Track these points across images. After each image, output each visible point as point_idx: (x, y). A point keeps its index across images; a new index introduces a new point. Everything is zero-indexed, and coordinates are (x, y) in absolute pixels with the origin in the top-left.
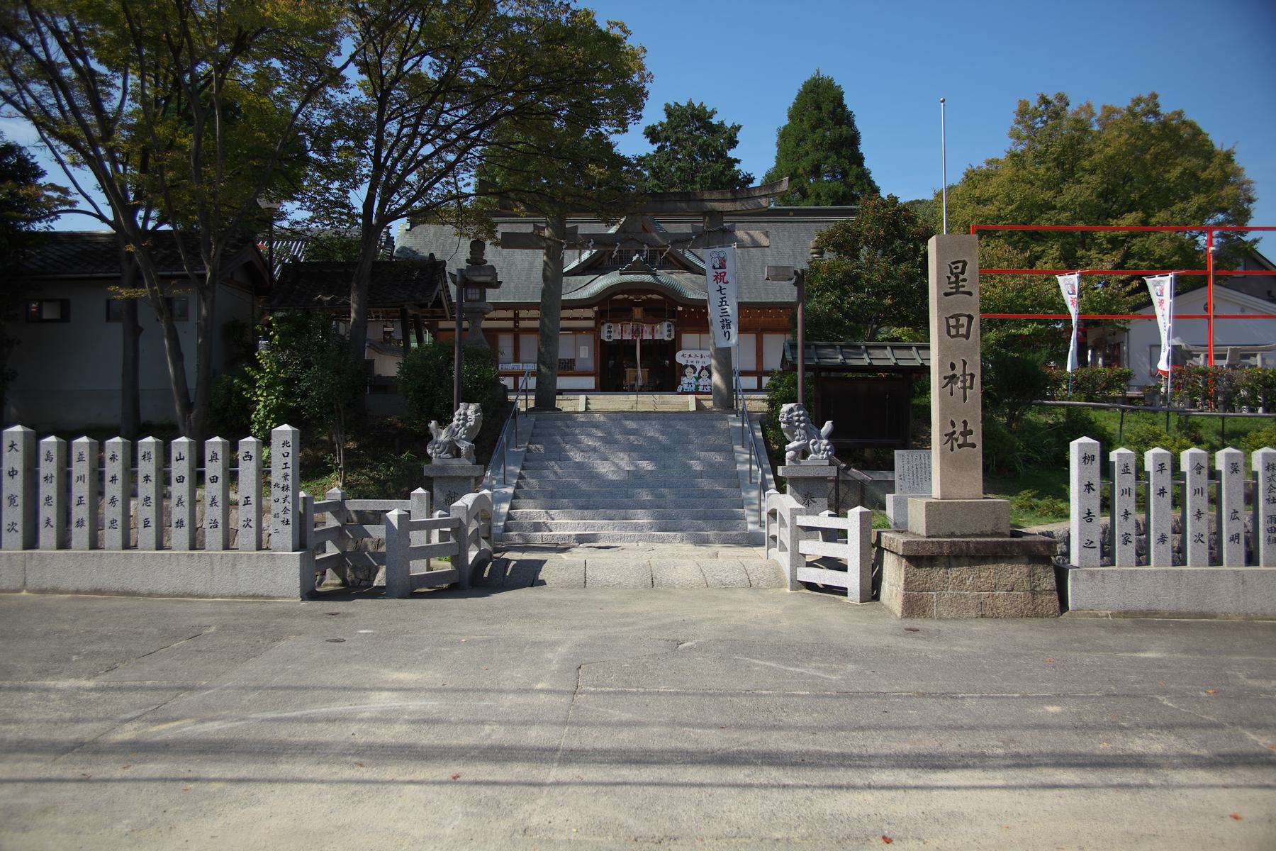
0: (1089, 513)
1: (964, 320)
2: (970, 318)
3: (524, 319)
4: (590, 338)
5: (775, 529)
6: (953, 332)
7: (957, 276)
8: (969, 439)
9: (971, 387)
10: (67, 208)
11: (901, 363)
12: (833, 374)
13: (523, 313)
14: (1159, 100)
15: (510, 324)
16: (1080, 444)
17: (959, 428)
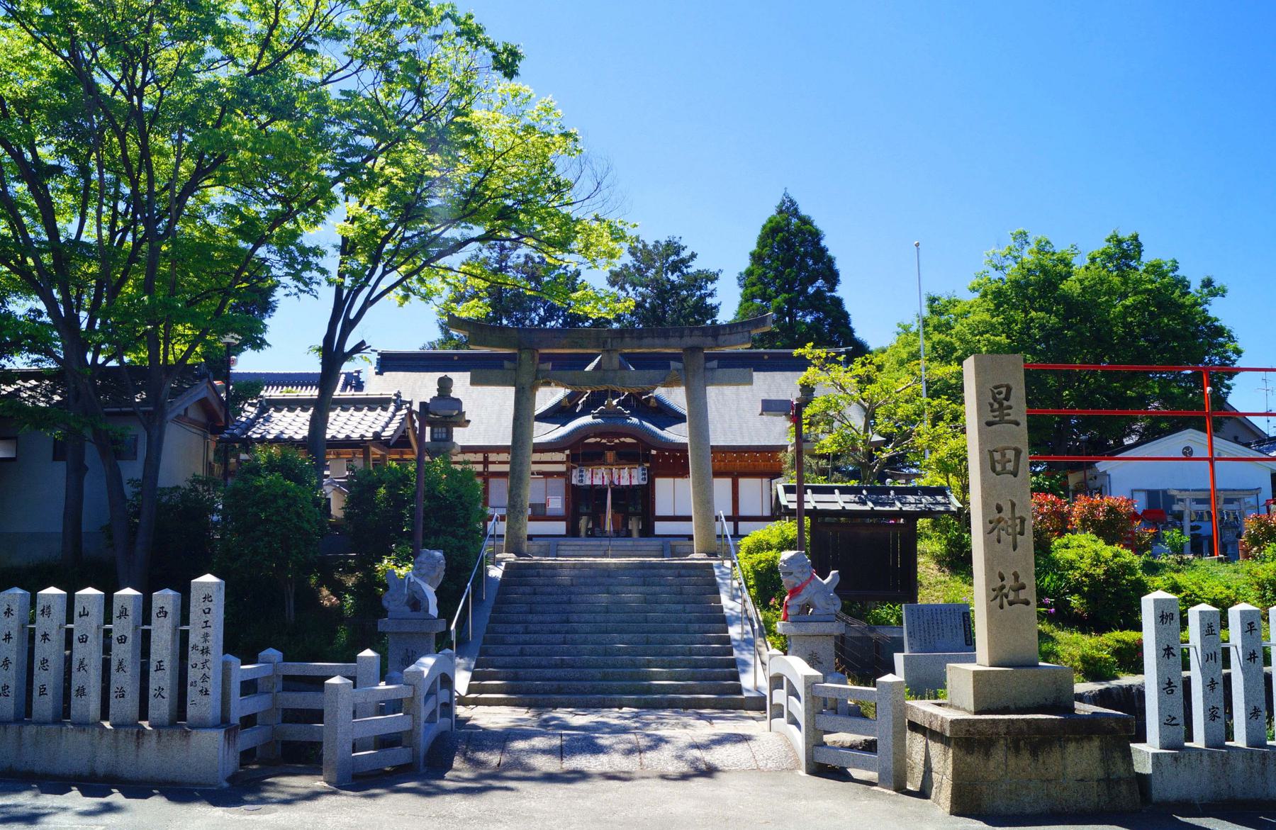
0: (1170, 683)
1: (1010, 454)
2: (1018, 452)
3: (494, 463)
5: (780, 696)
6: (999, 468)
8: (1023, 595)
9: (1022, 533)
10: (522, 774)
12: (827, 519)
15: (480, 468)
16: (1156, 601)
17: (1009, 582)
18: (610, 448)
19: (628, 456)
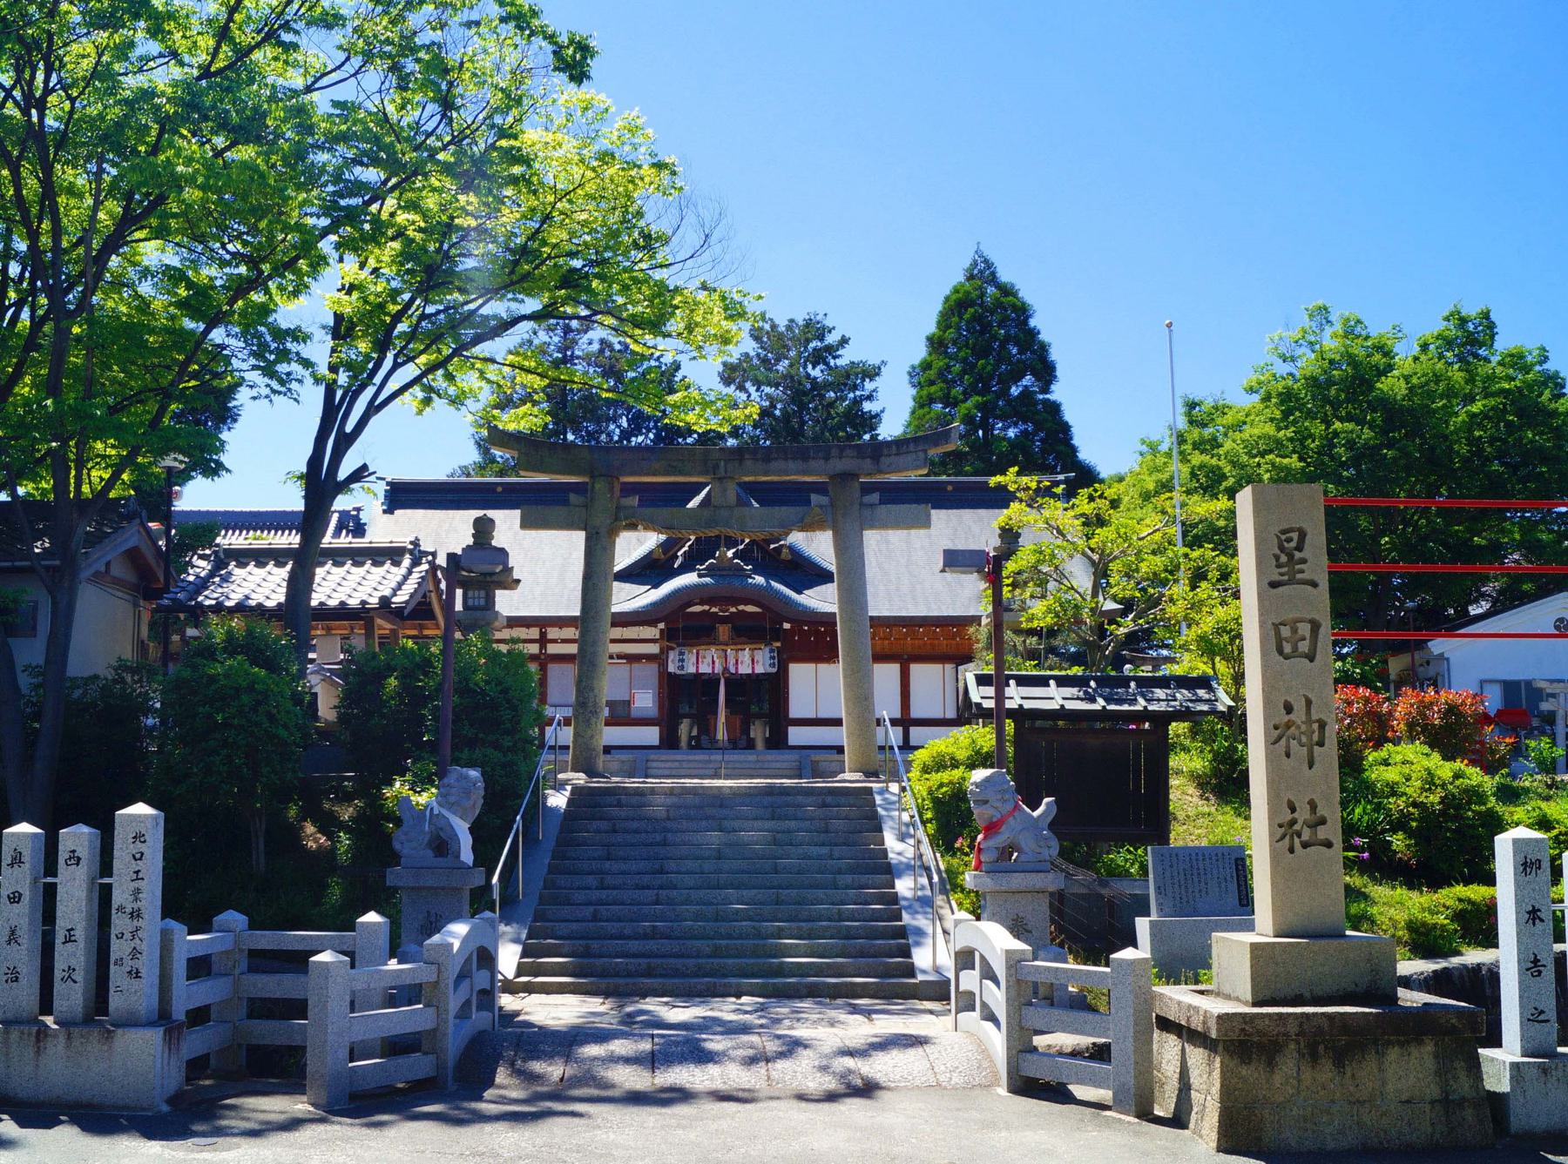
0: (1536, 961)
1: (1304, 629)
2: (1315, 626)
3: (554, 641)
4: (651, 670)
6: (1287, 649)
7: (1291, 556)
8: (1322, 833)
9: (1321, 744)
11: (1028, 705)
13: (553, 633)
14: (1493, 316)
16: (1516, 842)
17: (1303, 814)
18: (724, 620)
19: (749, 632)
